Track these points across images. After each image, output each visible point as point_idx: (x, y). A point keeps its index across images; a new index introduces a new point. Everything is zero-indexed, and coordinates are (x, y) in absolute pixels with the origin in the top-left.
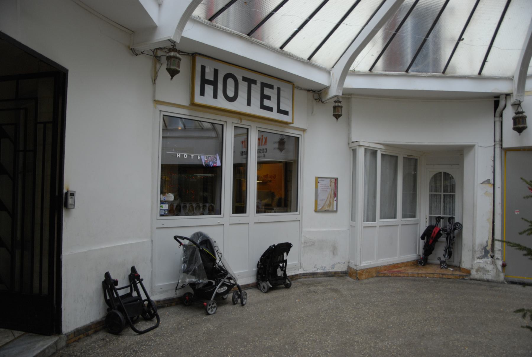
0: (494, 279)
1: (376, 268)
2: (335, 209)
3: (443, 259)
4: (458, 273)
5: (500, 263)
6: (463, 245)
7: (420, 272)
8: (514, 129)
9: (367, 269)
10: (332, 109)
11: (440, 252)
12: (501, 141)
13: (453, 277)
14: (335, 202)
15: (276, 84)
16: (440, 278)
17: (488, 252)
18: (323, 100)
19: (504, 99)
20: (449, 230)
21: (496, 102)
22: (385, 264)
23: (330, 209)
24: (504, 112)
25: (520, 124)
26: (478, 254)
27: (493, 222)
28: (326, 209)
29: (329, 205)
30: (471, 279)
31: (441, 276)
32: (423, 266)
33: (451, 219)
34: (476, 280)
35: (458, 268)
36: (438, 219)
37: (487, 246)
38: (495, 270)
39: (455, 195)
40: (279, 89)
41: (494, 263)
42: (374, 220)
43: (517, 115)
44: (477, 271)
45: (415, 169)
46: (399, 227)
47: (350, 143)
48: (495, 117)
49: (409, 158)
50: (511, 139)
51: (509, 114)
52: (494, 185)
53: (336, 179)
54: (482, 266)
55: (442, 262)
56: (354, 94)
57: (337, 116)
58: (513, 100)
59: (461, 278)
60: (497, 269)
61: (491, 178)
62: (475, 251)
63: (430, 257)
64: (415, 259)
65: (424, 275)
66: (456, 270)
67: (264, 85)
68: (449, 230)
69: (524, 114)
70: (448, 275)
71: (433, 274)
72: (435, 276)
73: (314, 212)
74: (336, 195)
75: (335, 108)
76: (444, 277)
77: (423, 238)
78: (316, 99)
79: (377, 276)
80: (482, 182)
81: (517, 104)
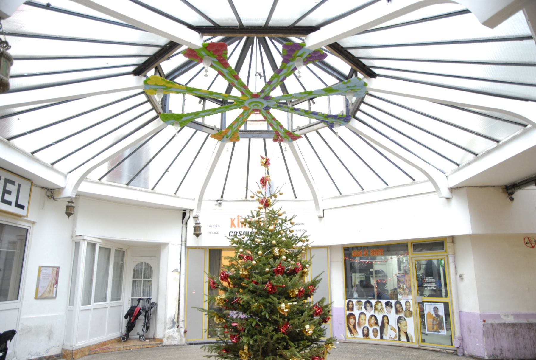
0: (179, 343)
1: (89, 347)
2: (54, 296)
3: (141, 333)
4: (153, 343)
5: (183, 330)
6: (158, 319)
7: (125, 345)
8: (194, 234)
9: (81, 348)
10: (65, 208)
11: (139, 327)
13: (150, 346)
14: (55, 289)
15: (18, 181)
17: (175, 323)
18: (55, 198)
20: (147, 309)
22: (96, 343)
23: (50, 295)
24: (188, 221)
25: (197, 231)
26: (169, 326)
28: (46, 296)
29: (49, 292)
30: (163, 346)
33: (148, 300)
34: (167, 346)
35: (154, 339)
36: (139, 300)
40: (19, 186)
41: (179, 331)
42: (89, 303)
44: (168, 338)
45: (123, 259)
46: (108, 309)
47: (74, 236)
49: (118, 250)
50: (192, 241)
53: (58, 268)
54: (171, 334)
56: (81, 195)
57: (69, 215)
58: (194, 214)
60: (181, 335)
63: (130, 333)
64: (119, 336)
65: (128, 348)
67: (7, 181)
68: (147, 309)
73: (34, 299)
74: (56, 282)
75: (68, 207)
76: (144, 347)
77: (126, 317)
78: (48, 196)
79: (89, 354)
81: (196, 218)
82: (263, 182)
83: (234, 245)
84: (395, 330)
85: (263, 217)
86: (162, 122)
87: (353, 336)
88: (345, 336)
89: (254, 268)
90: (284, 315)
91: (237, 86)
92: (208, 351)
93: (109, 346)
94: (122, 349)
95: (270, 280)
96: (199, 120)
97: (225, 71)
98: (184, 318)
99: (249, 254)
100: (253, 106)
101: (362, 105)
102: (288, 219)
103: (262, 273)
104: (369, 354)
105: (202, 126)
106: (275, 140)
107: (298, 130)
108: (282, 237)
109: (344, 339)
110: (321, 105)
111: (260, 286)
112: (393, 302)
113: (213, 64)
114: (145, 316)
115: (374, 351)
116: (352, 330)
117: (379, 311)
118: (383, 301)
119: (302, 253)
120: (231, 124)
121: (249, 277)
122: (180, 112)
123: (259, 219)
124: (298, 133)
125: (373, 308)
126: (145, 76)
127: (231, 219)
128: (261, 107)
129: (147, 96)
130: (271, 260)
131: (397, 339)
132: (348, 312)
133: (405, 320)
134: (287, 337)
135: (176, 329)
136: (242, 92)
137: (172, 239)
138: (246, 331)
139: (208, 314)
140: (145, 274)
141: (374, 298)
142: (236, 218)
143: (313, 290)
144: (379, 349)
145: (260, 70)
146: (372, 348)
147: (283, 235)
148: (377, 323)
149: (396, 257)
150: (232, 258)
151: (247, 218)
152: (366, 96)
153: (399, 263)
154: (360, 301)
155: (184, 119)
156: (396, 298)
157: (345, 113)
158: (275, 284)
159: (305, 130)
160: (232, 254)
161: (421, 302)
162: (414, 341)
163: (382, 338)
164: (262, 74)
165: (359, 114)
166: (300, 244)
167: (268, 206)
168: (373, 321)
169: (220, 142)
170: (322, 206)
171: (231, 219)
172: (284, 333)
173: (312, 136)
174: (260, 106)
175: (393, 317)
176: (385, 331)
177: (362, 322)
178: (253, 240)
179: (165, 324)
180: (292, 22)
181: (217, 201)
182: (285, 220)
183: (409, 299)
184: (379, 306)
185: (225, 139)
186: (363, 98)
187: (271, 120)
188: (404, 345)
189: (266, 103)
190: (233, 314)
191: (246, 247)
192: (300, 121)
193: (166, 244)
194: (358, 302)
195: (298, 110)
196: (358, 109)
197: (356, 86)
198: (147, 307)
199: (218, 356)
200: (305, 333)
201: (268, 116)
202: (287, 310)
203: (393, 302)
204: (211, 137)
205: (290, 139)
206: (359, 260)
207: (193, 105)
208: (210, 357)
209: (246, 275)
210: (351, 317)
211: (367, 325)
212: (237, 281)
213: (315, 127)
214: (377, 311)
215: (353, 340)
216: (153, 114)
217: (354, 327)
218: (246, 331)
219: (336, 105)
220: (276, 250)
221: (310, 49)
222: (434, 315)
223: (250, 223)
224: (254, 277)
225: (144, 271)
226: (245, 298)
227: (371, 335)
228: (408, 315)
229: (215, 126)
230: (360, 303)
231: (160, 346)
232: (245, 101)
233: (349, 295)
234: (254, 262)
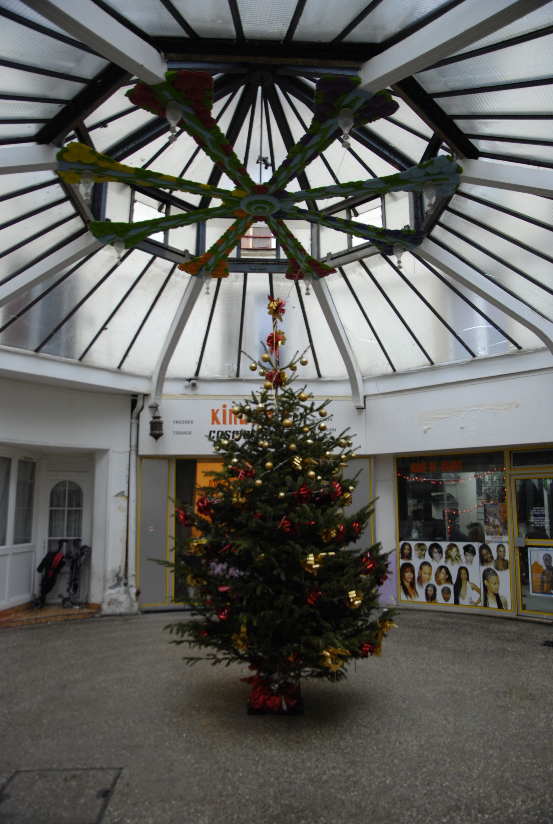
0: (128, 611)
3: (66, 595)
4: (86, 611)
5: (133, 591)
7: (38, 616)
8: (151, 435)
11: (62, 586)
12: (137, 446)
13: (80, 617)
16: (65, 620)
17: (121, 579)
19: (142, 400)
20: (74, 557)
21: (134, 400)
25: (156, 429)
26: (110, 583)
27: (127, 542)
30: (102, 616)
31: (66, 617)
32: (41, 607)
35: (86, 604)
36: (61, 542)
37: (120, 572)
38: (128, 600)
39: (82, 510)
41: (127, 592)
43: (155, 420)
44: (109, 604)
45: (32, 476)
46: (9, 557)
48: (131, 418)
50: (148, 446)
51: (146, 417)
52: (128, 498)
54: (114, 597)
55: (65, 600)
58: (151, 401)
59: (90, 616)
60: (131, 598)
61: (125, 489)
62: (107, 580)
63: (48, 596)
65: (43, 620)
66: (83, 608)
68: (74, 557)
69: (161, 419)
70: (75, 615)
71: (56, 616)
72: (59, 619)
76: (70, 618)
77: (40, 569)
80: (115, 494)
81: (154, 408)
82: (272, 343)
83: (222, 451)
84: (479, 591)
85: (273, 405)
86: (93, 239)
87: (410, 599)
88: (397, 598)
89: (258, 490)
90: (313, 573)
91: (229, 168)
92: (177, 633)
93: (12, 617)
94: (33, 622)
95: (287, 514)
96: (158, 237)
97: (207, 136)
98: (136, 571)
99: (248, 468)
100: (256, 209)
101: (446, 213)
102: (315, 407)
103: (274, 501)
104: (439, 629)
105: (161, 250)
106: (289, 277)
107: (329, 259)
108: (306, 438)
109: (395, 603)
110: (369, 215)
111: (269, 524)
112: (477, 545)
113: (186, 120)
114: (72, 568)
115: (445, 623)
116: (408, 589)
117: (453, 560)
118: (461, 545)
119: (341, 466)
120: (215, 245)
121: (250, 506)
122: (126, 220)
123: (266, 406)
124: (329, 264)
125: (444, 555)
126: (60, 145)
127: (213, 410)
128: (269, 212)
129: (66, 188)
130: (289, 478)
131: (481, 604)
132: (402, 562)
133: (496, 575)
134: (318, 613)
135: (122, 589)
136: (235, 182)
137: (115, 444)
138: (245, 603)
139: (176, 571)
140: (71, 501)
141: (444, 540)
142: (221, 409)
143: (361, 529)
144: (454, 621)
145: (266, 154)
146: (442, 619)
147: (308, 434)
148: (449, 579)
149: (473, 474)
150: (217, 474)
151: (244, 404)
152: (455, 195)
153: (479, 483)
154: (423, 545)
155: (132, 233)
156: (482, 540)
157: (412, 228)
158: (297, 520)
159: (341, 260)
160: (219, 468)
161: (523, 545)
162: (509, 607)
163: (457, 602)
164: (269, 161)
165: (437, 231)
166: (337, 451)
167: (281, 385)
168: (442, 575)
169: (195, 278)
170: (365, 389)
171: (213, 410)
172: (312, 606)
173: (354, 271)
174: (268, 208)
175: (476, 571)
176: (462, 592)
177: (425, 576)
178: (255, 444)
179: (105, 580)
180: (339, 29)
181: (189, 380)
182: (311, 410)
183: (503, 543)
184: (453, 553)
185: (203, 272)
186: (450, 198)
187: (286, 240)
188: (493, 614)
189: (278, 206)
190: (218, 568)
191: (243, 455)
192: (333, 241)
193: (104, 452)
194: (419, 545)
195: (335, 219)
196: (435, 221)
197: (441, 173)
198: (73, 553)
199: (193, 642)
200: (347, 605)
201: (281, 231)
202: (318, 566)
203: (477, 545)
204: (180, 268)
205: (315, 274)
206: (420, 477)
207: (147, 210)
208: (179, 643)
209: (243, 505)
210: (408, 569)
211: (433, 581)
212: (225, 513)
213: (359, 254)
214: (449, 561)
215: (410, 606)
216: (77, 224)
217: (412, 585)
218: (245, 603)
219: (397, 213)
220: (297, 461)
221: (369, 90)
222: (544, 568)
223: (249, 413)
224: (260, 508)
225: (69, 494)
226: (243, 544)
227: (440, 597)
228: (501, 566)
229: (187, 251)
230: (422, 547)
231: (97, 615)
232: (241, 199)
233: (404, 534)
234: (259, 482)
